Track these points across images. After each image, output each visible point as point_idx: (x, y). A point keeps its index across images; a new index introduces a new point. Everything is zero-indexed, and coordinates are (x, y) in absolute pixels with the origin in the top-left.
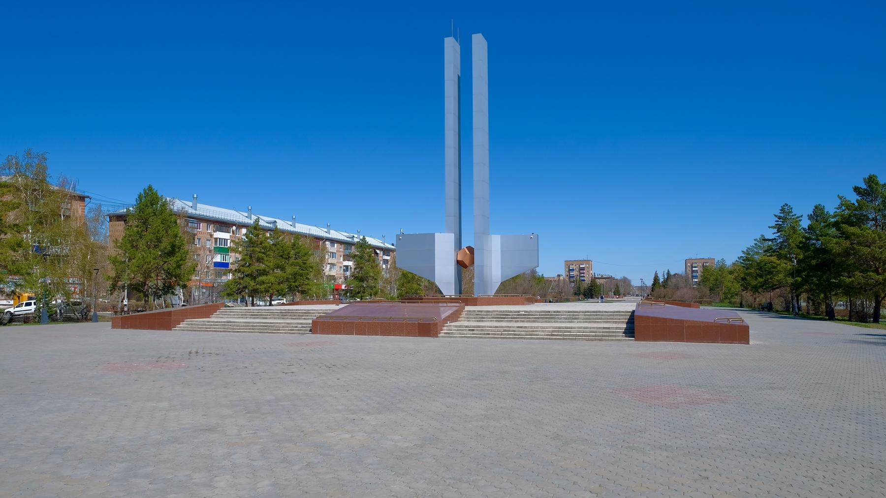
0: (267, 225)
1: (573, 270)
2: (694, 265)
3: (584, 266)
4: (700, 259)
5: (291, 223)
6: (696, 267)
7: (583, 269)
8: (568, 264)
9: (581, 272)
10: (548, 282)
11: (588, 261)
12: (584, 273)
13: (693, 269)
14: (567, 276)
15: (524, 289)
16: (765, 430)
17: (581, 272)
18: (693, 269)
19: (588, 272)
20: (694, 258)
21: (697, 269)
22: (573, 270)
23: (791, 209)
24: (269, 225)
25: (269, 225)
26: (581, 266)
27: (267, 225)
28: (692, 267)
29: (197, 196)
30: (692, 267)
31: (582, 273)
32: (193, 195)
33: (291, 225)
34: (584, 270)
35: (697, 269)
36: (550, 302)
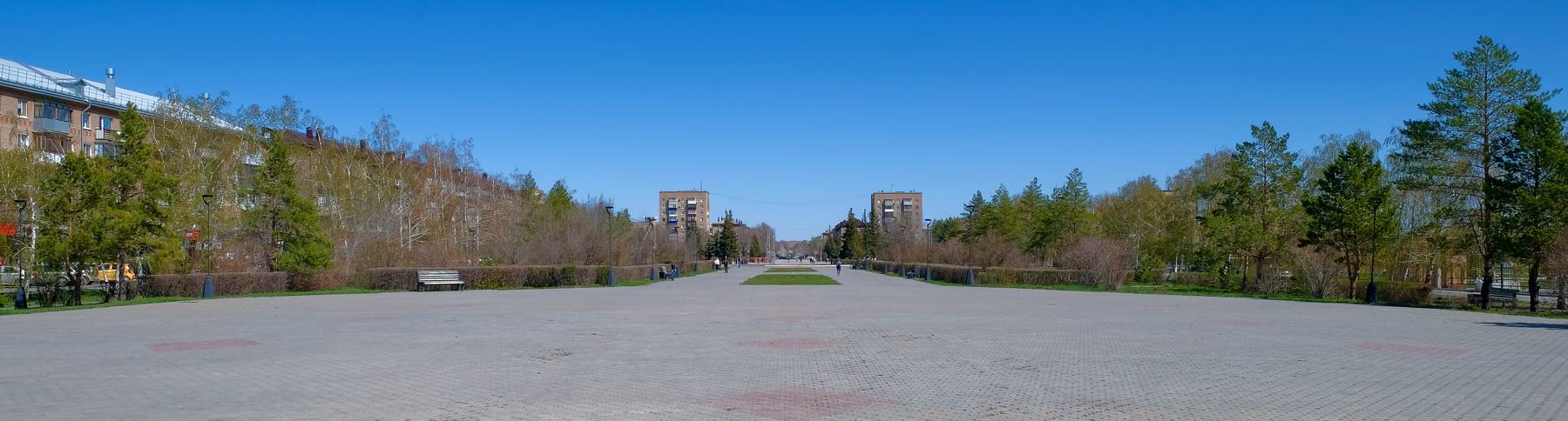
0: (59, 88)
1: (675, 209)
2: (887, 203)
3: (694, 202)
4: (897, 193)
5: (103, 86)
6: (890, 208)
7: (693, 208)
8: (665, 197)
9: (690, 212)
10: (632, 224)
11: (702, 194)
12: (695, 215)
13: (886, 210)
14: (664, 220)
15: (589, 238)
16: (1080, 403)
17: (690, 212)
18: (886, 210)
19: (702, 212)
20: (888, 191)
21: (892, 210)
22: (675, 209)
23: (1080, 174)
24: (66, 90)
25: (66, 90)
26: (689, 202)
27: (59, 88)
28: (884, 207)
29: (114, 70)
30: (884, 207)
31: (691, 215)
32: (107, 70)
33: (104, 91)
34: (695, 209)
35: (892, 210)
36: (662, 276)
